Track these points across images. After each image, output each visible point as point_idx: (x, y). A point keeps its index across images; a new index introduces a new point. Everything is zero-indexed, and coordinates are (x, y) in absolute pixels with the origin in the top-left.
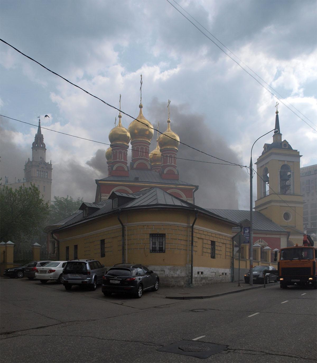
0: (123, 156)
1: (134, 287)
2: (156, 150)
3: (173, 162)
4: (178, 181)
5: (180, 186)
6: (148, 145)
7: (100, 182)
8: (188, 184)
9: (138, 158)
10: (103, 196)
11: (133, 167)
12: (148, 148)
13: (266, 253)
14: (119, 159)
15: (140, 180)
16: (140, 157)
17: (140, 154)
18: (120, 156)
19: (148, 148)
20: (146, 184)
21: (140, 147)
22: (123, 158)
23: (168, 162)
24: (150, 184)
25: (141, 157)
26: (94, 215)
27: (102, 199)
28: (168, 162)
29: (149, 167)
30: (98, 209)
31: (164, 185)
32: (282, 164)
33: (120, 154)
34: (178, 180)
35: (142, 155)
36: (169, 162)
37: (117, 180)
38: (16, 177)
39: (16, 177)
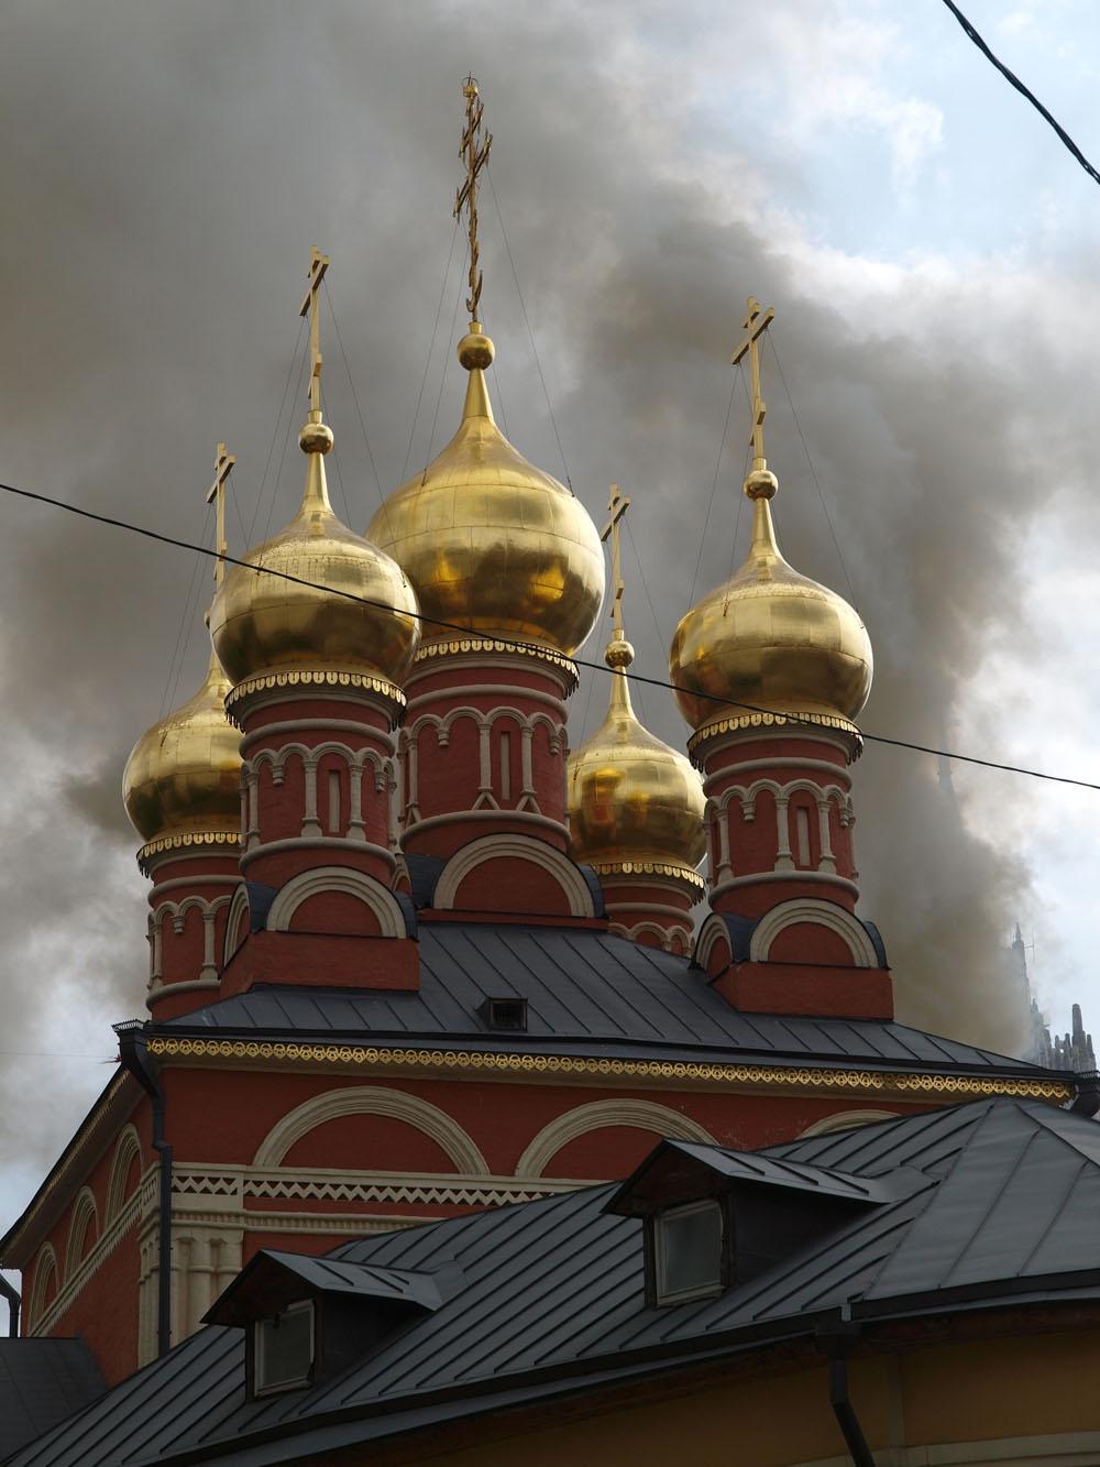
0: (357, 802)
2: (638, 753)
3: (827, 852)
4: (889, 1028)
5: (929, 1084)
6: (553, 699)
7: (157, 1047)
8: (997, 1062)
10: (190, 1190)
11: (429, 905)
12: (559, 727)
14: (323, 824)
15: (535, 1028)
16: (486, 805)
17: (486, 784)
19: (559, 727)
20: (605, 1068)
21: (486, 719)
22: (356, 817)
23: (784, 849)
24: (636, 1061)
25: (498, 811)
26: (365, 1388)
27: (181, 1213)
28: (784, 849)
29: (581, 902)
30: (402, 1316)
31: (773, 1069)
33: (505, 743)
34: (889, 1021)
35: (506, 795)
36: (795, 858)
37: (318, 1024)
38: (618, 598)
39: (618, 598)
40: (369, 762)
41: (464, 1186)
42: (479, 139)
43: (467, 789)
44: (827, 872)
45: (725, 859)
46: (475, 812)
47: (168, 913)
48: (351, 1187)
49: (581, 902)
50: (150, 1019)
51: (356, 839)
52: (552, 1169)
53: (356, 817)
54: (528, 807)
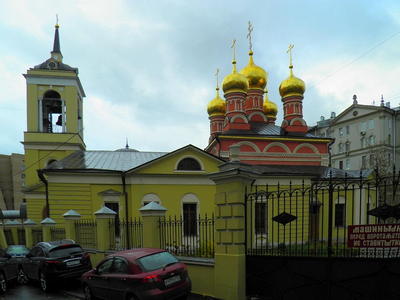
1: (78, 278)
9: (253, 110)
11: (290, 125)
13: (10, 231)
14: (237, 109)
16: (254, 108)
18: (238, 106)
21: (254, 97)
22: (241, 108)
25: (255, 109)
29: (266, 120)
32: (43, 90)
40: (243, 101)
41: (303, 155)
42: (251, 28)
43: (252, 106)
44: (299, 114)
45: (286, 113)
46: (253, 109)
47: (213, 123)
48: (303, 155)
49: (266, 120)
50: (203, 142)
51: (241, 111)
52: (297, 152)
53: (241, 108)
54: (259, 108)
